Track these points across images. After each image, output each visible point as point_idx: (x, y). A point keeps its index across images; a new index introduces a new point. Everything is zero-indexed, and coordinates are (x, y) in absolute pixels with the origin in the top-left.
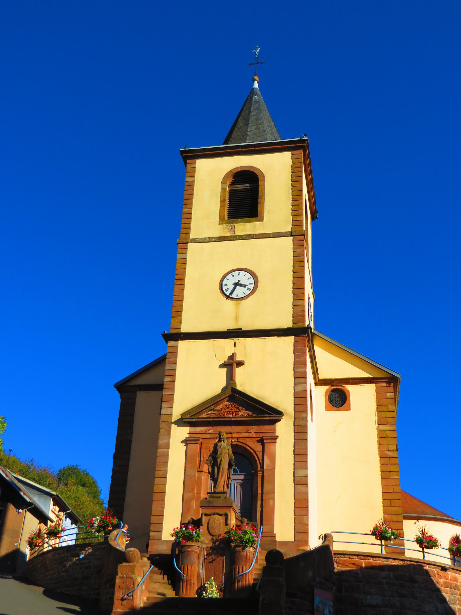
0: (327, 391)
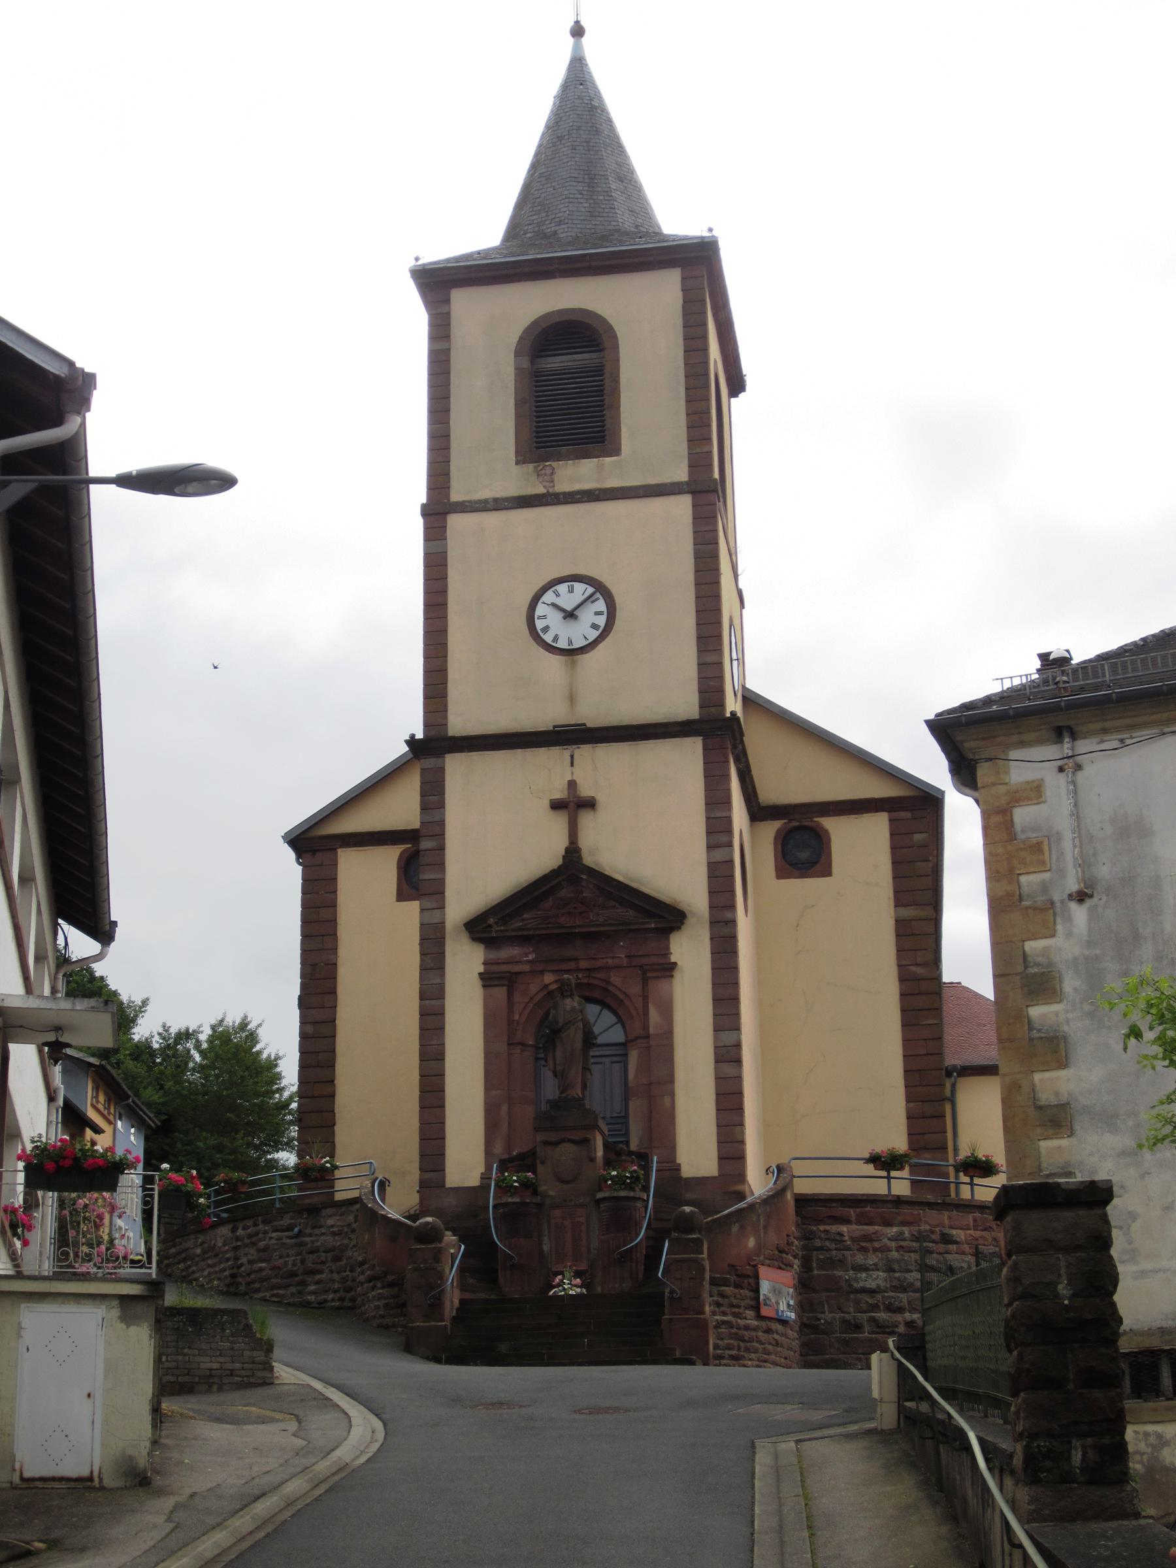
0: (778, 832)
